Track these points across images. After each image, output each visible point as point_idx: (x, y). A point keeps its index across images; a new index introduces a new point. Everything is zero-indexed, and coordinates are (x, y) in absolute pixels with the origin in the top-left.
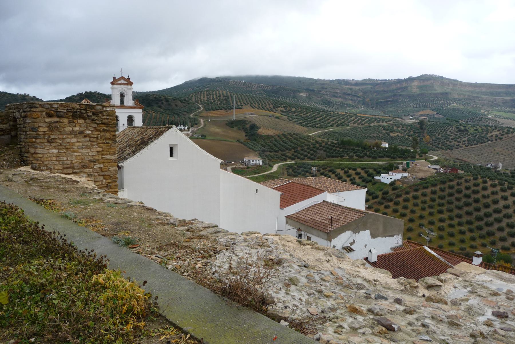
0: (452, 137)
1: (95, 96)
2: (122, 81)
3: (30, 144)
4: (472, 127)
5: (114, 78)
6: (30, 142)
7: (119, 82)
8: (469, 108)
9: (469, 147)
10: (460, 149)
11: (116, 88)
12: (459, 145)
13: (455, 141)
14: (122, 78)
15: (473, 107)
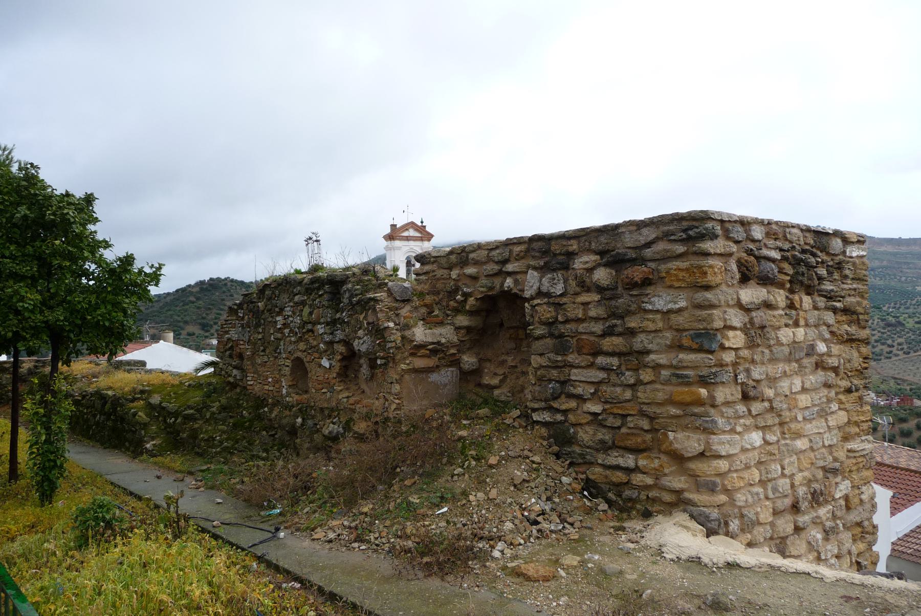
0: (876, 337)
1: (226, 285)
2: (412, 233)
3: (674, 411)
4: (909, 317)
5: (393, 226)
6: (671, 402)
7: (406, 234)
8: (893, 284)
9: (912, 354)
10: (894, 358)
11: (399, 248)
12: (891, 352)
13: (883, 344)
14: (412, 225)
15: (900, 281)
